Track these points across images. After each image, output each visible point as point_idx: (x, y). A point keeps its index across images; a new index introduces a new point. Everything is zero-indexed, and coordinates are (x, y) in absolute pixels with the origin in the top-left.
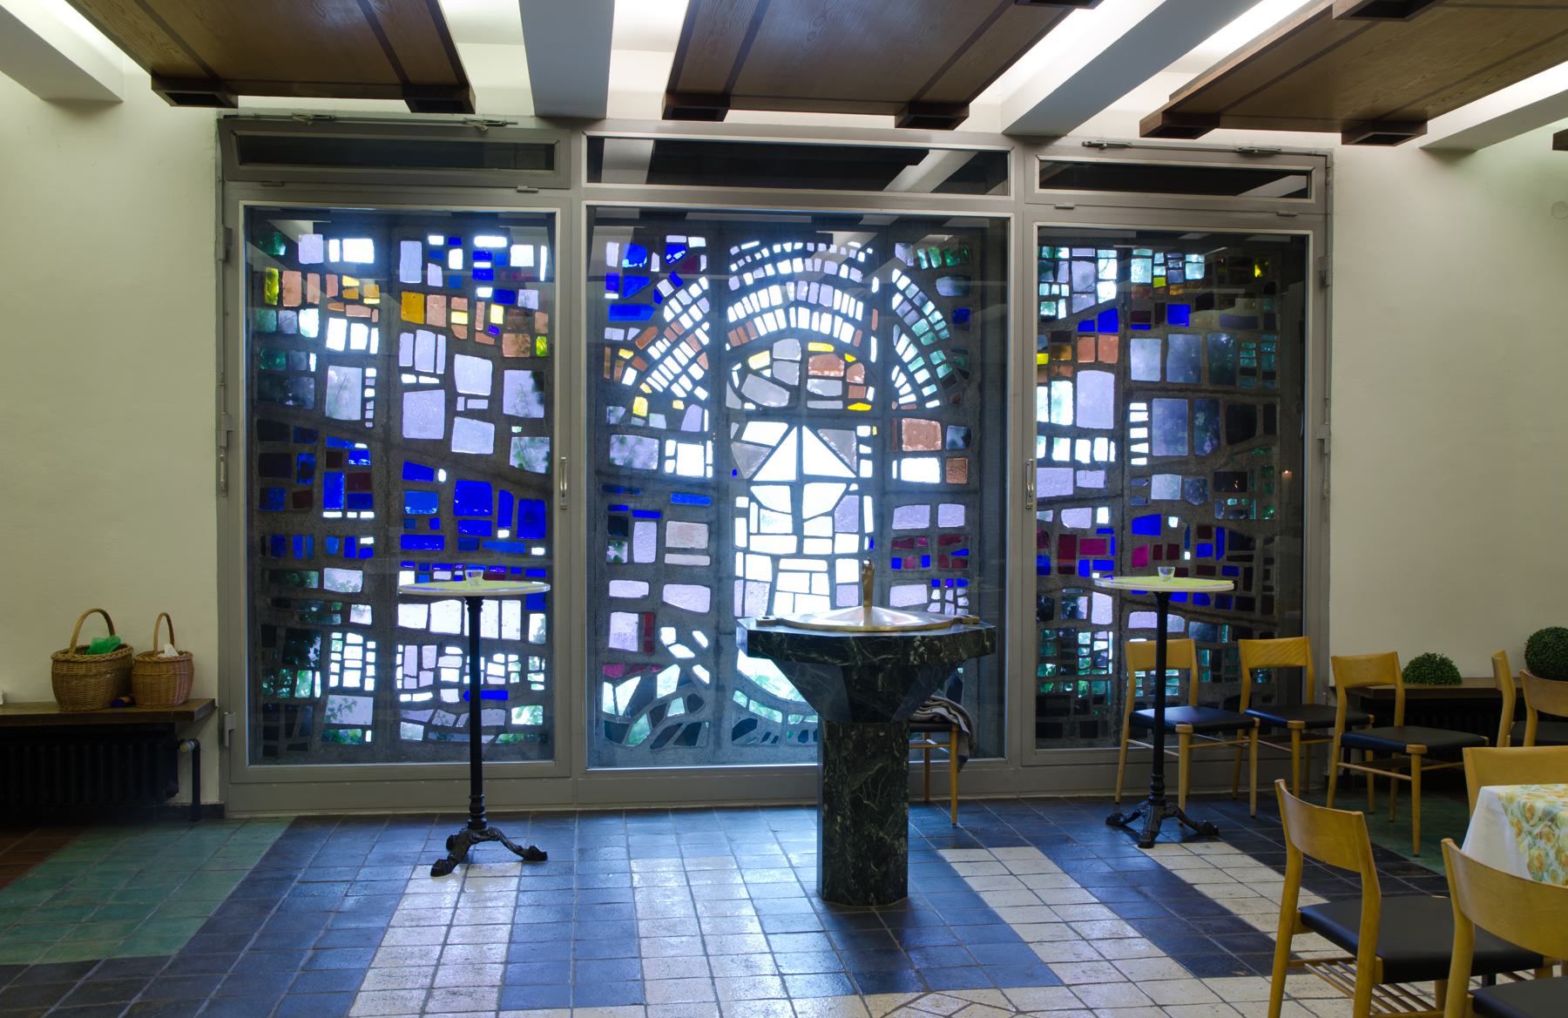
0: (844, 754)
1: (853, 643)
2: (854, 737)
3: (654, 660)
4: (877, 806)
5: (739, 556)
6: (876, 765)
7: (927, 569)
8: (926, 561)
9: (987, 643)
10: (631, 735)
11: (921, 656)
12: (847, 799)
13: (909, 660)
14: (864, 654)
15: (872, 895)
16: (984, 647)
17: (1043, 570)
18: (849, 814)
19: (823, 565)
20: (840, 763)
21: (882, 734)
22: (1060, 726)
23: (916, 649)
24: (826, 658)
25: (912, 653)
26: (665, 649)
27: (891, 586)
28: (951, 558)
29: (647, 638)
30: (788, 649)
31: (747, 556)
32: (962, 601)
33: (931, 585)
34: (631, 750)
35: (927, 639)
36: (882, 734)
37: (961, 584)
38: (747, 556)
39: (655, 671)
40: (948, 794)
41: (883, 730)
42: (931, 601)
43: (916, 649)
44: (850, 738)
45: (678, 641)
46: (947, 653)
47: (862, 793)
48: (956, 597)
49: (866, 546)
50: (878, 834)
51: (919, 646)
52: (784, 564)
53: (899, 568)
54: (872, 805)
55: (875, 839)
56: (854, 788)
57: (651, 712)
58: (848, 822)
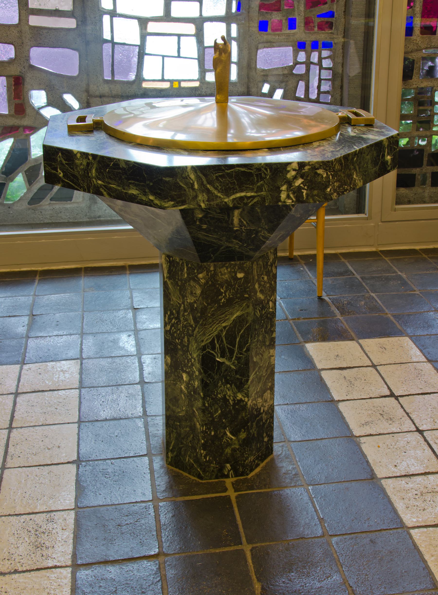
0: (190, 299)
1: (192, 176)
2: (203, 281)
3: (26, 122)
4: (233, 364)
5: (106, 19)
6: (232, 314)
7: (293, 31)
8: (292, 24)
9: (389, 158)
10: (8, 192)
11: (298, 191)
12: (195, 356)
13: (278, 199)
14: (208, 192)
15: (228, 465)
16: (385, 163)
17: (409, 31)
18: (197, 373)
19: (191, 28)
20: (185, 310)
21: (240, 275)
22: (413, 176)
23: (290, 183)
24: (151, 198)
25: (284, 188)
26: (37, 112)
27: (257, 49)
28: (318, 20)
29: (17, 101)
30: (98, 178)
31: (114, 19)
32: (326, 63)
33: (296, 47)
34: (9, 206)
35: (307, 168)
36: (240, 275)
37: (327, 46)
38: (114, 19)
39: (28, 133)
40: (314, 248)
41: (242, 269)
42: (296, 63)
43: (290, 183)
44: (197, 281)
45: (49, 104)
46: (336, 184)
47: (214, 348)
48: (320, 59)
49: (234, 9)
50: (235, 397)
51: (295, 178)
52: (152, 27)
53: (266, 30)
54: (227, 363)
55: (231, 403)
56: (203, 344)
57: (26, 172)
58: (196, 383)
